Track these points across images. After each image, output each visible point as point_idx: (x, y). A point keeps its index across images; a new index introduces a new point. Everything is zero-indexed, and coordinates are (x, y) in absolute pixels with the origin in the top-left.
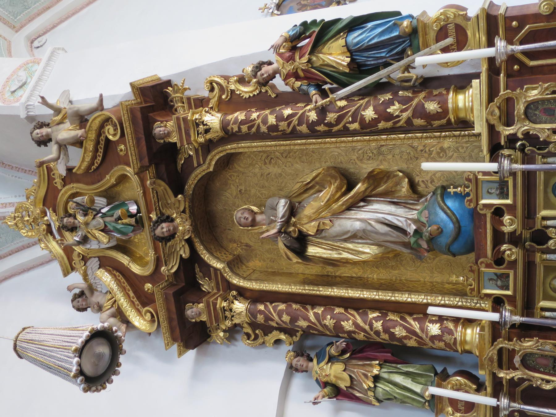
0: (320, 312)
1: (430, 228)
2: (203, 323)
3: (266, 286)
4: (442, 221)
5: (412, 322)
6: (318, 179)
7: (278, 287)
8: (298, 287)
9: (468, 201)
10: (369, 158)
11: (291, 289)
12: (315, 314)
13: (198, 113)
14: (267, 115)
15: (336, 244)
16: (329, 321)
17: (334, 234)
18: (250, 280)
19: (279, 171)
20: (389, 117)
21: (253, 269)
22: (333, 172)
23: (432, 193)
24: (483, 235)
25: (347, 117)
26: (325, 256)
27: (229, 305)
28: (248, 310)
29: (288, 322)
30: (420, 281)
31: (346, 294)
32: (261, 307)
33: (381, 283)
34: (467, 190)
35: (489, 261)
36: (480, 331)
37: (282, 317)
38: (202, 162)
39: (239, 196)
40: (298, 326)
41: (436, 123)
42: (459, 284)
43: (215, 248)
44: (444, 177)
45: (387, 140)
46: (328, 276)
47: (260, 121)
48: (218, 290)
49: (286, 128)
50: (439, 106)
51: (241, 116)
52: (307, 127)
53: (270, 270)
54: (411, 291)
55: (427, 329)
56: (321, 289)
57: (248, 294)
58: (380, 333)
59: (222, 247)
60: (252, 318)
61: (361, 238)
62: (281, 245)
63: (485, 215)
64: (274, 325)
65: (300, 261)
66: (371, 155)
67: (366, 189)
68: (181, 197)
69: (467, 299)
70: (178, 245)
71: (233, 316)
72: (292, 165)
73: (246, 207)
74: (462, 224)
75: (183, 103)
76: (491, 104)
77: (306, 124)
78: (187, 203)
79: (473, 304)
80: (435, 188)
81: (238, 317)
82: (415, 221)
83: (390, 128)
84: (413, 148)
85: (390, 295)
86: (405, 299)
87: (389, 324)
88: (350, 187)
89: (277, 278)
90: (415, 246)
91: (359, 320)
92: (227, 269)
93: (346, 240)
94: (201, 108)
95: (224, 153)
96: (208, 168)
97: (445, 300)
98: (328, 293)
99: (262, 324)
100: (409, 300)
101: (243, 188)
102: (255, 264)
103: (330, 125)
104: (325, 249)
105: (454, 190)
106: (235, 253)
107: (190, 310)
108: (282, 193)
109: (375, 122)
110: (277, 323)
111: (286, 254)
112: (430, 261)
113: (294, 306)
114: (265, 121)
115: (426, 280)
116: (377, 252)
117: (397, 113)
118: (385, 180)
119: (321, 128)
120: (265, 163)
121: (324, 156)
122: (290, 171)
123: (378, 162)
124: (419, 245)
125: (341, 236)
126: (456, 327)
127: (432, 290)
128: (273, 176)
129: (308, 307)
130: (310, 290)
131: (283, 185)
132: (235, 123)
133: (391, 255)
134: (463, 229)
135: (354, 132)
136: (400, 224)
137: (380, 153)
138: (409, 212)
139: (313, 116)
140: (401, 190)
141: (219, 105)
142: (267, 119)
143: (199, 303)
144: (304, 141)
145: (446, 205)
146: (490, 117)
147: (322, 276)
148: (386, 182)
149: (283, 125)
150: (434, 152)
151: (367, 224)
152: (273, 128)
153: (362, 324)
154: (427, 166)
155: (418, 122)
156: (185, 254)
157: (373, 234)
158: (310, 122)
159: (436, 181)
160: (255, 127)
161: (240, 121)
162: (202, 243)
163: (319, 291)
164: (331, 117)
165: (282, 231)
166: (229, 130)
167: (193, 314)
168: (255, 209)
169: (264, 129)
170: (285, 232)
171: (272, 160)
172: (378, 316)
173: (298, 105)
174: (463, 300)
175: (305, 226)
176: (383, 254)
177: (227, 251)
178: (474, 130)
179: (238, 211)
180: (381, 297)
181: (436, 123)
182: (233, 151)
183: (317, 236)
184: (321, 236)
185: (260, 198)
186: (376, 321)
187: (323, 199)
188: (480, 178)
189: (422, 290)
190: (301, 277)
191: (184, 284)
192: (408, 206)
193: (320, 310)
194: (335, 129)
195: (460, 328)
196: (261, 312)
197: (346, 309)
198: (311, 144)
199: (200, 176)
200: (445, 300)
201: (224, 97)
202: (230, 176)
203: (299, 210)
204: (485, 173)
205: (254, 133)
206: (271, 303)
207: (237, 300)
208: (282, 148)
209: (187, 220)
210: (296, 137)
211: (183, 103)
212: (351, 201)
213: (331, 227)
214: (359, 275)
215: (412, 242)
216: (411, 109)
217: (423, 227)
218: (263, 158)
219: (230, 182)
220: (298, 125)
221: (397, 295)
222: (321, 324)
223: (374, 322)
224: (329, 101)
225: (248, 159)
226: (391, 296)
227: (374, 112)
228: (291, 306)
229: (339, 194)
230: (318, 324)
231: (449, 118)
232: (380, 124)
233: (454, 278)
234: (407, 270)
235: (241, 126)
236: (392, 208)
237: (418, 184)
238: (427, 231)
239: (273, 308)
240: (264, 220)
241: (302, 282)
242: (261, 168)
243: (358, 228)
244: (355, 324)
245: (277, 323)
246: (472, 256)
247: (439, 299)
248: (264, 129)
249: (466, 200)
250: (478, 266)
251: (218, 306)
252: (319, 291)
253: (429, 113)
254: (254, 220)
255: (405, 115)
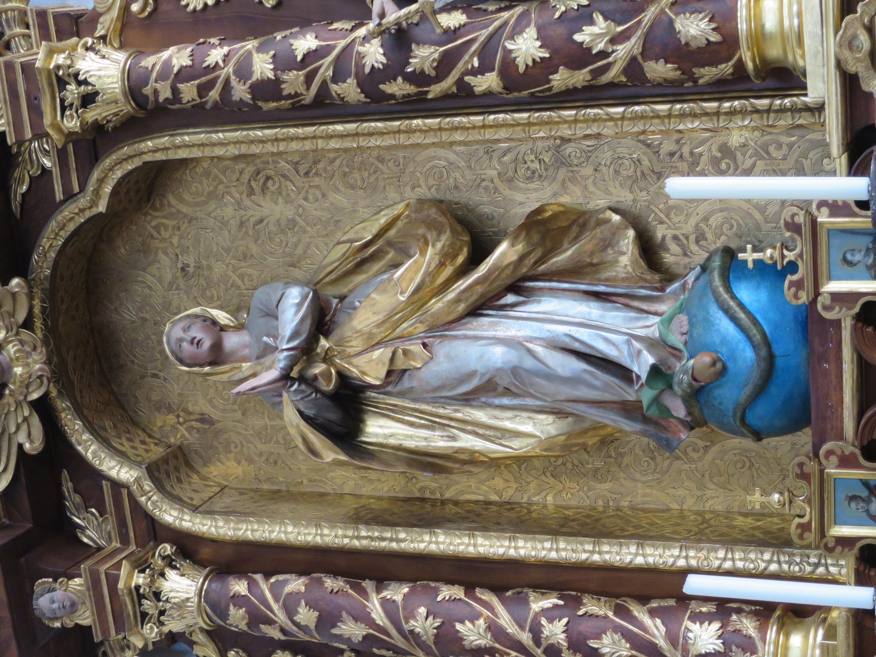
0: (398, 598)
1: (692, 362)
2: (84, 631)
3: (253, 531)
4: (724, 341)
5: (647, 620)
6: (392, 233)
7: (286, 533)
8: (340, 532)
9: (792, 284)
10: (532, 176)
11: (322, 535)
12: (384, 602)
13: (63, 51)
14: (249, 54)
15: (441, 411)
16: (423, 623)
17: (435, 383)
18: (210, 513)
19: (289, 212)
20: (581, 57)
21: (219, 485)
22: (433, 212)
23: (698, 269)
24: (833, 378)
25: (466, 57)
26: (410, 444)
27: (153, 581)
28: (204, 596)
29: (312, 626)
30: (669, 510)
31: (471, 549)
32: (240, 587)
33: (566, 518)
34: (790, 256)
35: (849, 449)
36: (826, 637)
37: (297, 612)
38: (76, 189)
39: (181, 282)
40: (339, 638)
41: (707, 74)
42: (771, 515)
43: (115, 426)
44: (732, 226)
45: (576, 121)
46: (423, 500)
47: (230, 69)
48: (125, 541)
49: (302, 89)
50: (713, 25)
51: (178, 57)
52: (359, 85)
53: (266, 487)
54: (642, 537)
55: (685, 638)
56: (402, 535)
57: (205, 552)
58: (561, 651)
59: (136, 424)
60: (215, 618)
61: (507, 392)
62: (290, 415)
63: (837, 324)
64: (277, 635)
65: (343, 457)
66: (536, 165)
67: (522, 258)
68: (18, 285)
69: (792, 555)
70: (12, 417)
71: (162, 613)
72: (324, 195)
73: (197, 310)
74: (777, 350)
75: (27, 27)
76: (848, 18)
77: (357, 76)
78: (37, 302)
79: (809, 569)
80: (706, 255)
81: (176, 614)
82: (652, 344)
83: (584, 88)
84: (649, 146)
85: (589, 547)
86: (628, 559)
87: (585, 627)
88: (479, 251)
89: (285, 507)
90: (653, 412)
91: (505, 619)
92: (148, 485)
93: (467, 399)
94: (75, 39)
95: (137, 163)
96: (94, 203)
97: (733, 560)
98: (422, 546)
99: (241, 634)
100: (640, 560)
101: (191, 260)
102: (226, 469)
103: (419, 79)
104: (411, 424)
105: (757, 256)
106: (172, 440)
107: (47, 596)
108: (297, 273)
109: (542, 69)
110: (283, 631)
111: (305, 440)
112: (695, 456)
113: (330, 583)
114: (244, 70)
115: (685, 507)
116: (552, 430)
117: (601, 46)
118: (573, 234)
119: (398, 88)
120: (251, 192)
121: (410, 168)
122: (318, 213)
123: (556, 186)
124: (669, 408)
125: (453, 387)
126: (762, 630)
127: (701, 532)
128: (272, 228)
129: (368, 585)
130: (372, 539)
131: (299, 251)
132: (161, 77)
133: (591, 440)
134: (780, 363)
135: (489, 101)
136: (611, 352)
137: (561, 162)
138: (638, 319)
139: (374, 54)
140: (617, 261)
141: (122, 30)
142: (250, 65)
143: (70, 577)
144: (351, 127)
145: (734, 297)
146: (846, 54)
147: (407, 500)
148: (576, 239)
149: (293, 80)
150: (704, 159)
151: (524, 352)
152: (267, 89)
153: (512, 629)
154: (679, 186)
155: (659, 70)
156: (32, 442)
157: (539, 380)
158: (367, 70)
159: (709, 236)
160: (219, 86)
161: (176, 70)
162: (79, 411)
163: (398, 541)
164: (424, 56)
165: (294, 374)
166: (146, 97)
167: (55, 606)
168: (222, 317)
169: (241, 91)
170: (302, 379)
171: (270, 183)
172: (556, 606)
173: (335, 26)
174: (782, 558)
175: (355, 361)
176: (570, 435)
177: (150, 436)
178: (806, 95)
179: (174, 324)
180: (563, 554)
181: (707, 74)
182: (160, 156)
183: (389, 388)
184: (399, 388)
185: (238, 288)
186: (551, 621)
187: (404, 285)
188: (822, 223)
189: (674, 532)
190: (351, 504)
191: (30, 526)
192: (636, 304)
193: (398, 593)
194: (435, 90)
195: (772, 633)
196: (238, 600)
197: (469, 589)
198: (371, 134)
199: (71, 227)
200: (733, 560)
201: (135, 7)
202: (157, 228)
203: (340, 318)
204: (836, 208)
205: (216, 105)
206: (267, 575)
207: (174, 568)
208: (294, 146)
209: (35, 348)
210: (330, 117)
211: (27, 27)
212: (479, 289)
213: (426, 363)
214: (507, 496)
215: (645, 402)
216: (639, 33)
217: (673, 360)
218: (246, 177)
219: (155, 243)
220: (335, 79)
221: (606, 548)
222: (400, 630)
223: (544, 621)
224: (417, 11)
225: (205, 181)
226: (592, 552)
227: (538, 43)
228: (320, 582)
229: (448, 271)
230: (393, 632)
231: (740, 59)
232: (556, 77)
233: (756, 499)
234: (635, 480)
235: (180, 86)
236: (592, 310)
237: (663, 246)
238: (683, 369)
239: (272, 589)
240: (246, 346)
241: (350, 518)
242: (239, 204)
243: (499, 364)
244: (494, 629)
245: (283, 631)
246: (805, 438)
247: (718, 557)
248: (241, 91)
249: (787, 283)
250: (820, 463)
251: (121, 585)
252: (398, 541)
253: (687, 44)
254: (217, 347)
255: (622, 51)
